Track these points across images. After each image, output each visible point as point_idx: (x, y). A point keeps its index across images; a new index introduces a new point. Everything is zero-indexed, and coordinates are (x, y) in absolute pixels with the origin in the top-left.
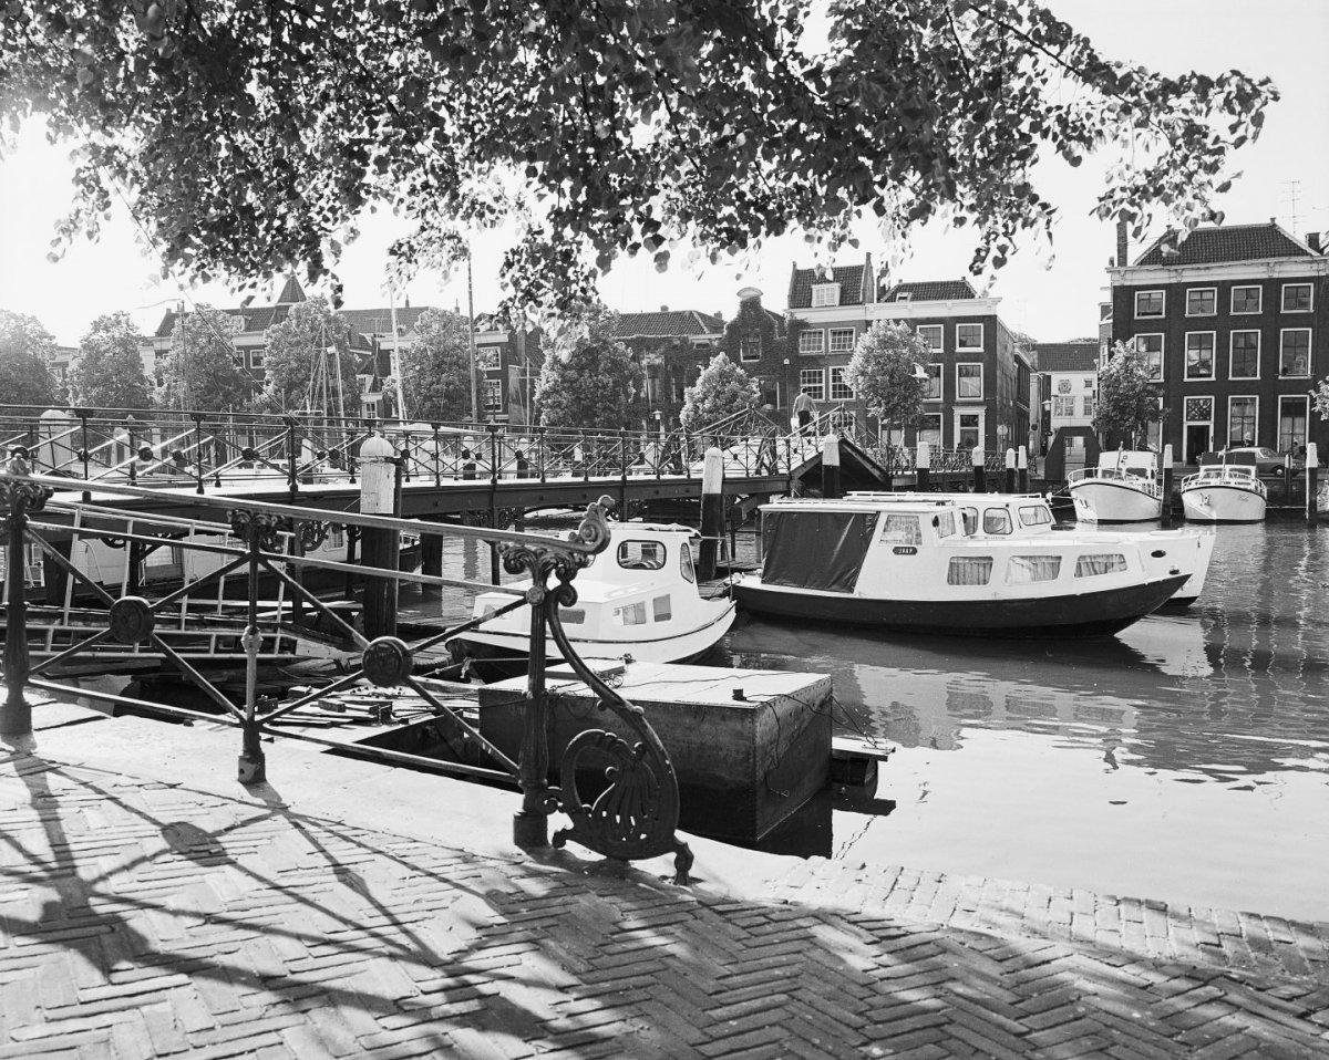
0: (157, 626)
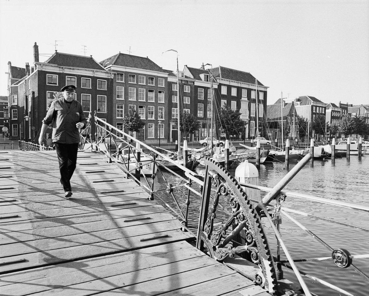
0: (314, 112)
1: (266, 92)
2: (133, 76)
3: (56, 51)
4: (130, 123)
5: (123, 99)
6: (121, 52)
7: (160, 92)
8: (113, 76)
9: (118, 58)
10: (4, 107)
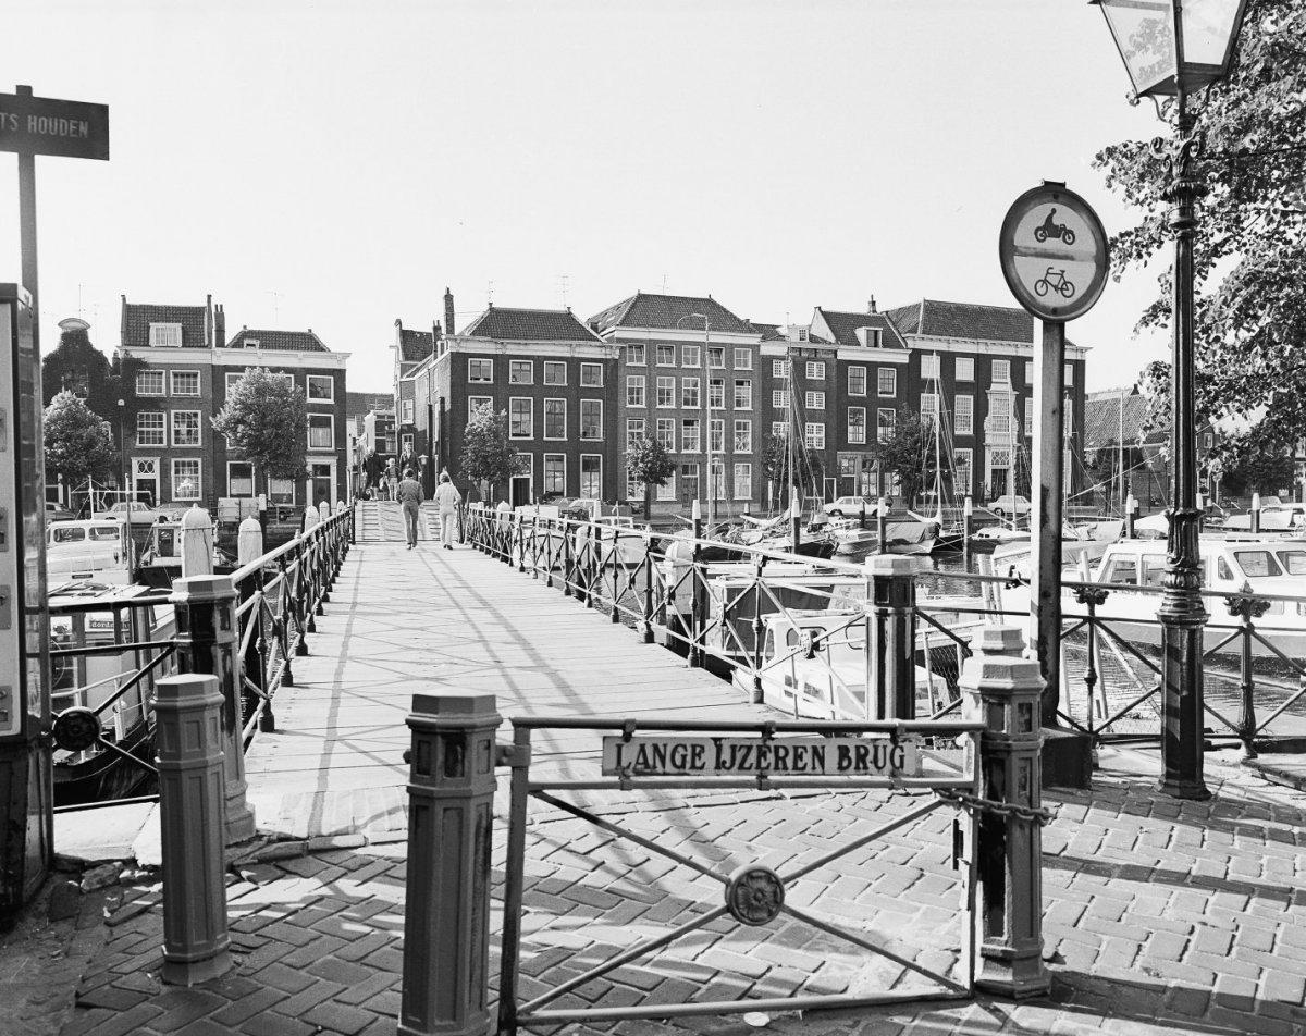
1: (1083, 362)
2: (670, 349)
3: (491, 304)
4: (641, 465)
5: (644, 406)
6: (642, 292)
7: (740, 383)
8: (618, 352)
9: (633, 306)
10: (387, 427)
